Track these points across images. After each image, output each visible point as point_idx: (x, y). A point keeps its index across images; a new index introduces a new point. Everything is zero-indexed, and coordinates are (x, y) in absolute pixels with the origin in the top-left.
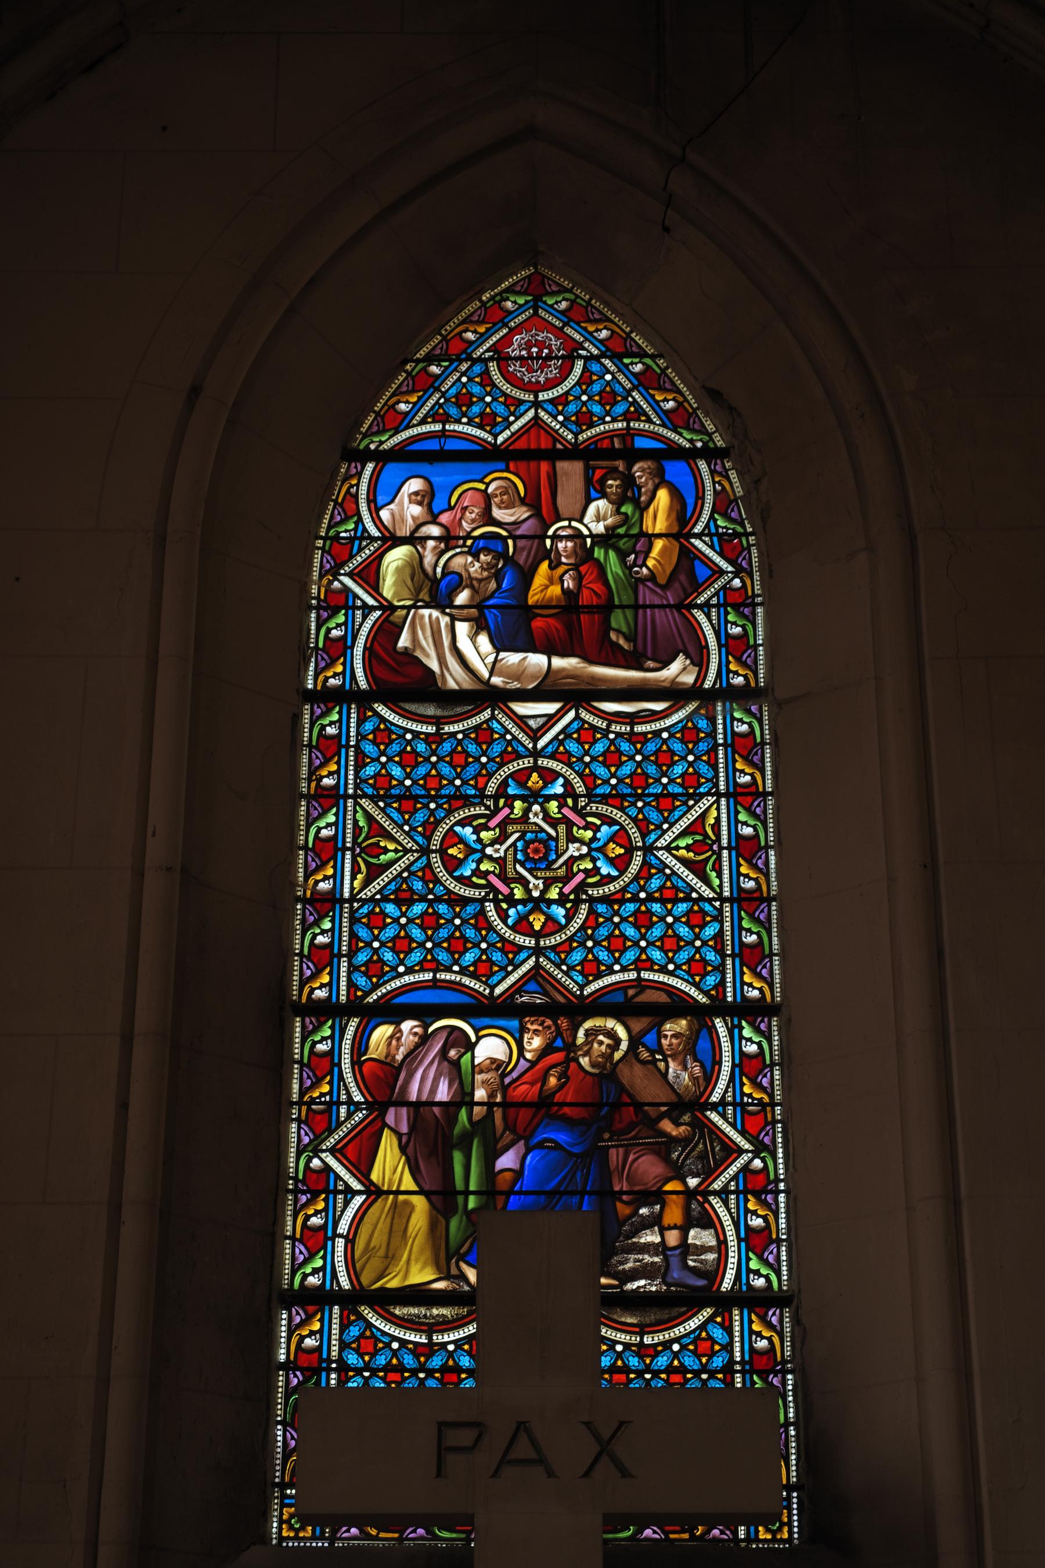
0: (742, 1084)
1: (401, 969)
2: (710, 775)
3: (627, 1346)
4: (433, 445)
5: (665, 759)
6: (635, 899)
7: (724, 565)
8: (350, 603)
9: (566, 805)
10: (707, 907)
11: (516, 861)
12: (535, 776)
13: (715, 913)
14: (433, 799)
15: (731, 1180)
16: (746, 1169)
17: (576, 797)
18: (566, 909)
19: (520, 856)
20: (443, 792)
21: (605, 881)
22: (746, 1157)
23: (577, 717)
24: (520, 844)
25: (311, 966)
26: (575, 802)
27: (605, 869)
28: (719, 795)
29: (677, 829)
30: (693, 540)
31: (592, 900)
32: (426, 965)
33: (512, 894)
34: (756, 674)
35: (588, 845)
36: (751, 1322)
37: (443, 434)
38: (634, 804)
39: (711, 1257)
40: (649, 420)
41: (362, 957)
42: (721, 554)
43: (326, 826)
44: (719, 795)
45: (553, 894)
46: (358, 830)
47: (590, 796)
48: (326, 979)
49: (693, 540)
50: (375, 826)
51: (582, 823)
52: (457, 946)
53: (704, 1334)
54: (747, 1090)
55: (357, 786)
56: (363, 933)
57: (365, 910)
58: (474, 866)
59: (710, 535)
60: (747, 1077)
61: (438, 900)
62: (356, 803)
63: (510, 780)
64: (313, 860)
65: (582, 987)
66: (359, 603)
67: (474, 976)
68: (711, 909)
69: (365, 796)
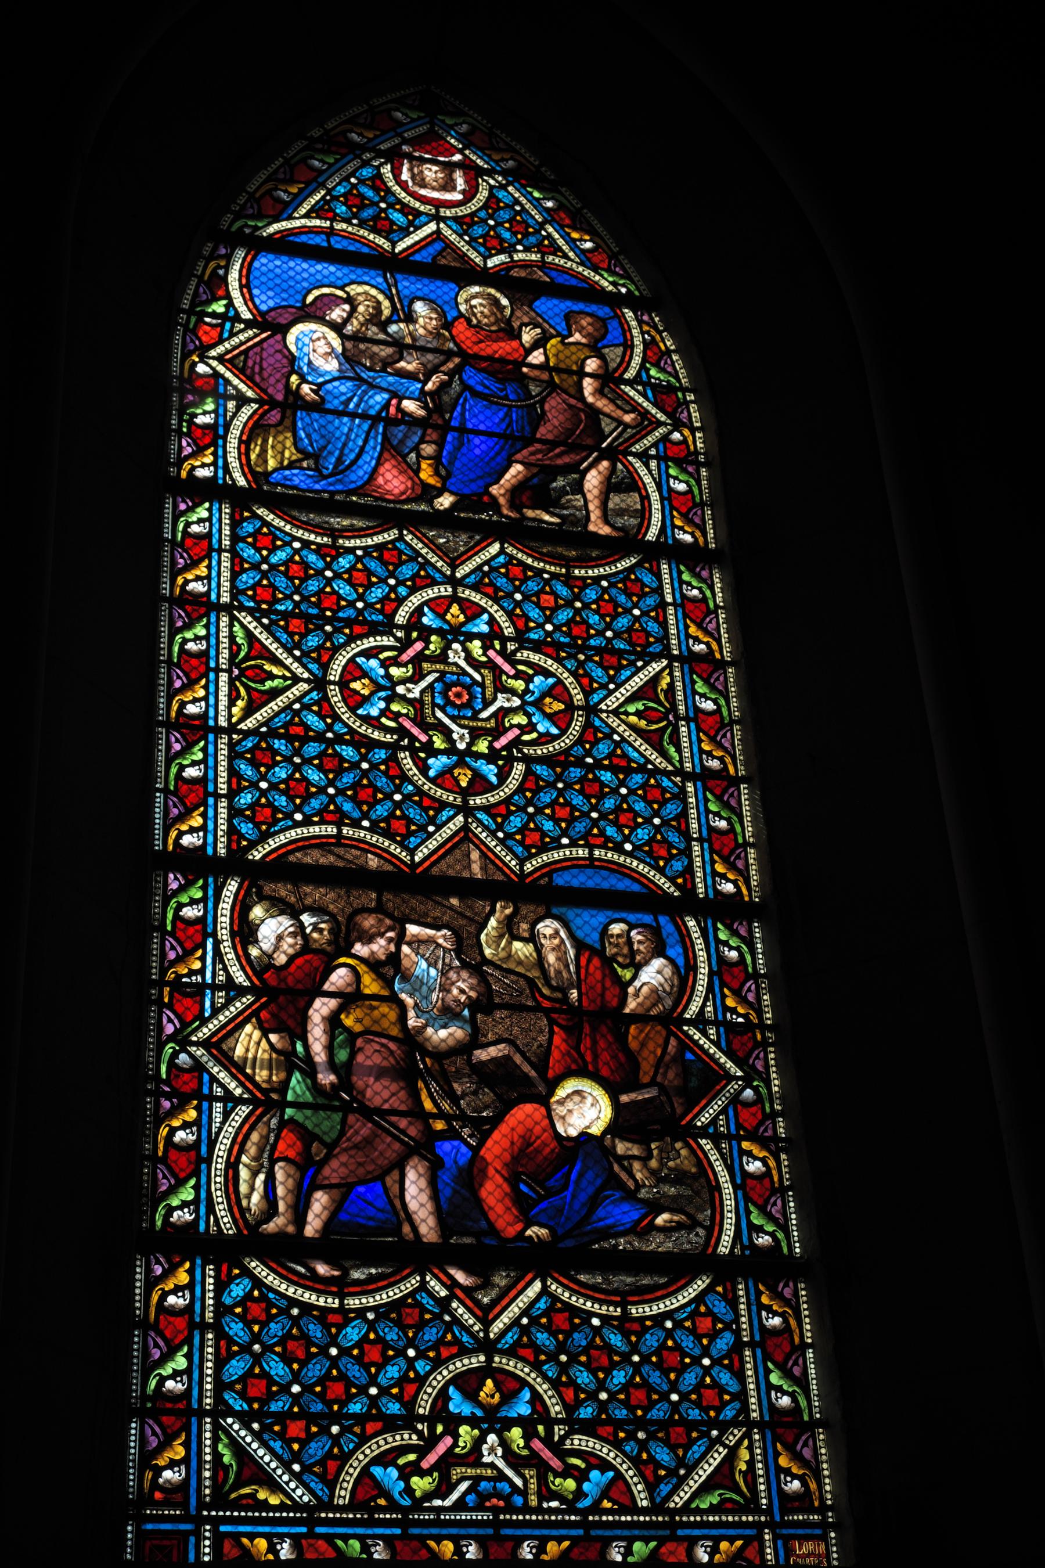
0: (724, 997)
1: (298, 817)
2: (654, 585)
3: (605, 1319)
4: (319, 240)
5: (671, 1360)
6: (580, 763)
7: (661, 416)
8: (206, 1091)
9: (536, 1434)
10: (666, 783)
11: (434, 705)
12: (455, 609)
13: (676, 790)
14: (329, 621)
15: (720, 1113)
16: (665, 438)
17: (550, 1423)
18: (497, 766)
19: (439, 700)
20: (341, 614)
21: (543, 740)
22: (662, 430)
23: (544, 1291)
24: (438, 686)
25: (161, 1343)
26: (550, 1432)
27: (544, 726)
28: (672, 658)
29: (693, 1484)
30: (630, 458)
31: (527, 760)
32: (328, 817)
33: (430, 742)
34: (704, 534)
35: (521, 697)
36: (700, 741)
37: (331, 232)
38: (631, 1436)
39: (634, 522)
40: (565, 256)
41: (245, 799)
42: (655, 404)
43: (193, 638)
44: (750, 1424)
45: (482, 746)
46: (221, 1474)
47: (521, 638)
48: (179, 1452)
49: (630, 458)
50: (256, 645)
51: (512, 672)
52: (364, 795)
53: (703, 1309)
54: (730, 1002)
55: (233, 597)
56: (246, 770)
57: (249, 744)
58: (382, 705)
59: (644, 385)
60: (729, 989)
61: (339, 739)
62: (216, 1427)
63: (451, 1389)
64: (165, 1177)
65: (522, 862)
66: (219, 1091)
67: (387, 834)
68: (670, 785)
69: (242, 608)
